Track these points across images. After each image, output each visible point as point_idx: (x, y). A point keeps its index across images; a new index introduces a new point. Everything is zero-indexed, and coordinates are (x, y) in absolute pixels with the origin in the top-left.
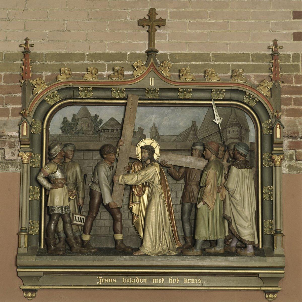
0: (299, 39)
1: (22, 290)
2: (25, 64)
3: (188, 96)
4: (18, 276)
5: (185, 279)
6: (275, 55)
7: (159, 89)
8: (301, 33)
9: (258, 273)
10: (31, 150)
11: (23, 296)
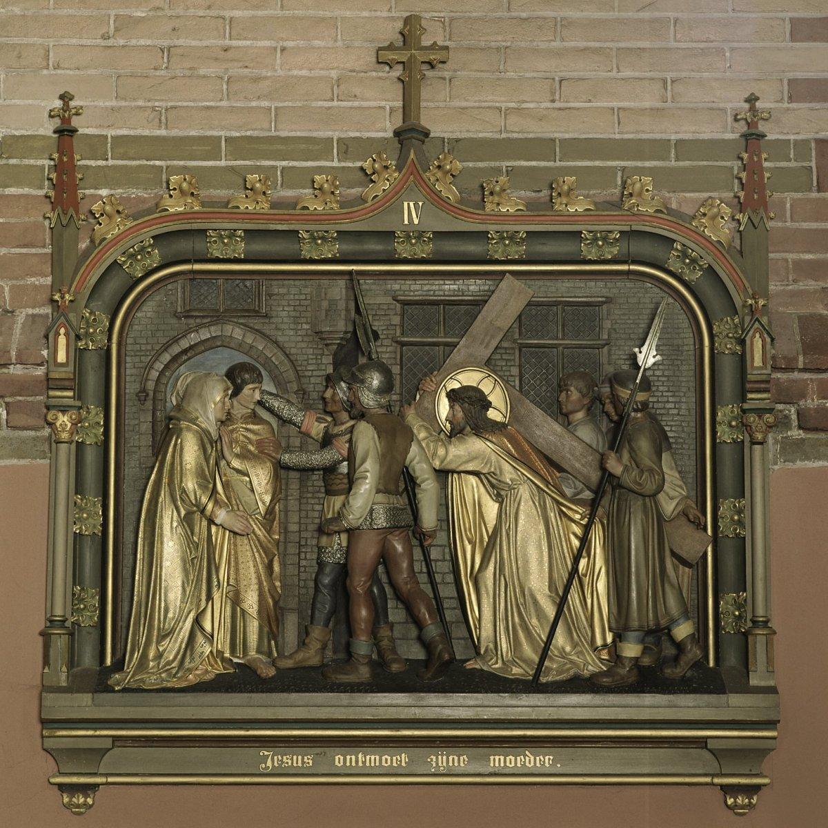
3: (610, 253)
4: (44, 749)
7: (434, 233)
8: (825, 80)
9: (702, 743)
10: (78, 403)
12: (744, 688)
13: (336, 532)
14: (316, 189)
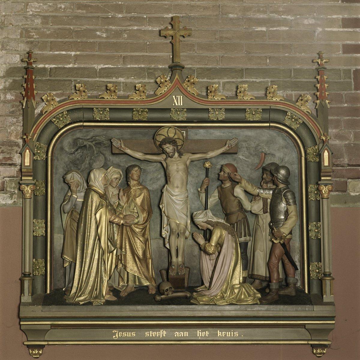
1: (26, 346)
5: (218, 331)
7: (187, 109)
9: (304, 326)
13: (288, 235)
14: (77, 90)
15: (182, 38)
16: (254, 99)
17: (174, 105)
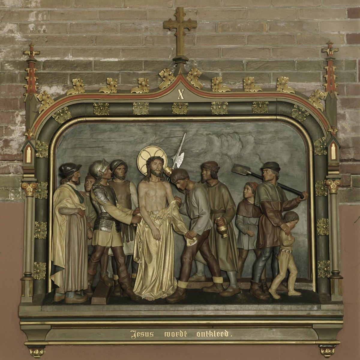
0: (357, 42)
2: (29, 75)
6: (330, 60)
7: (189, 103)
9: (312, 324)
11: (320, 353)
12: (328, 301)
15: (186, 31)
16: (261, 91)
17: (179, 98)
